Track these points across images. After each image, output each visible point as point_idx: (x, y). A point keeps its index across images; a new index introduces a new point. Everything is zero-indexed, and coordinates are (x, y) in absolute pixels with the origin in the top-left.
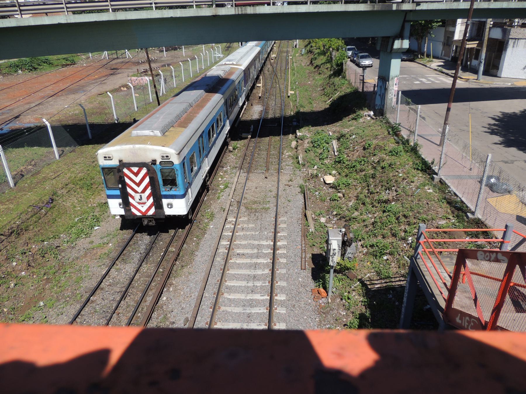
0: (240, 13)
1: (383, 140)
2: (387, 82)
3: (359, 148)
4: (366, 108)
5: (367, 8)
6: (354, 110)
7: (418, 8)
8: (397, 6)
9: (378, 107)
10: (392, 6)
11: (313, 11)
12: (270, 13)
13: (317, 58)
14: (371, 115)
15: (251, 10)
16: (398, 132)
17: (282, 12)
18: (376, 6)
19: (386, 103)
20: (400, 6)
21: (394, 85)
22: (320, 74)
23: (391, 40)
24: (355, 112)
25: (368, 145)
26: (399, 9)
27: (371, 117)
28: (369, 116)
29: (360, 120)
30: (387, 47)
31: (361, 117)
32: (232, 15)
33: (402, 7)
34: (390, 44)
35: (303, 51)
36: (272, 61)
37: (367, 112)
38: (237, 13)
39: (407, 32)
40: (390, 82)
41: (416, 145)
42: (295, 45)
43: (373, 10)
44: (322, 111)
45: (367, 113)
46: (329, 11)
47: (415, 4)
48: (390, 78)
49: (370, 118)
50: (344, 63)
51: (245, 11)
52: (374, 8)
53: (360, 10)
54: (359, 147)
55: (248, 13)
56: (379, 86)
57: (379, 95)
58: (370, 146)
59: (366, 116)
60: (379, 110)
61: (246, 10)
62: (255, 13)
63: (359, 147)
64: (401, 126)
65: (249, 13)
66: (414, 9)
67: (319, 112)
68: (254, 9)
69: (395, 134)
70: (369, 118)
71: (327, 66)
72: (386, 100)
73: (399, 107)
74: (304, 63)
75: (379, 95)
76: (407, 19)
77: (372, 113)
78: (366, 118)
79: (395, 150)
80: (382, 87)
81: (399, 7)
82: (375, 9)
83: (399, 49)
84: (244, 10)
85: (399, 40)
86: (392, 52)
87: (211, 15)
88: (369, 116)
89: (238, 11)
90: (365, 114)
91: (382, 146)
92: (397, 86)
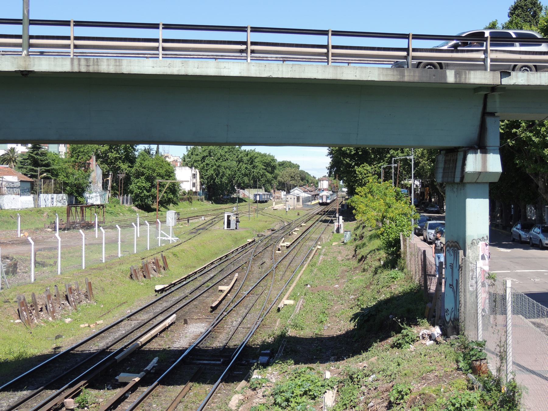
0: (83, 69)
1: (439, 382)
2: (461, 252)
3: (379, 404)
4: (425, 321)
5: (387, 75)
6: (395, 323)
7: (506, 81)
8: (457, 74)
9: (449, 316)
10: (445, 76)
11: (258, 76)
12: (161, 73)
13: (367, 244)
14: (436, 335)
15: (108, 65)
16: (478, 363)
17: (182, 72)
18: (406, 73)
19: (462, 302)
20: (463, 76)
21: (478, 259)
22: (364, 270)
23: (460, 156)
24: (399, 330)
25: (396, 395)
26: (463, 81)
27: (435, 340)
28: (431, 337)
29: (409, 348)
30: (455, 172)
31: (413, 341)
32: (65, 72)
33: (469, 79)
34: (459, 164)
35: (347, 236)
36: (277, 252)
37: (427, 329)
38: (76, 69)
39: (493, 139)
40: (468, 251)
41: (513, 389)
42: (335, 229)
43: (401, 80)
44: (338, 337)
45: (428, 332)
46: (297, 76)
47: (498, 74)
48: (468, 242)
49: (432, 342)
50: (401, 238)
51: (96, 67)
52: (404, 76)
53: (369, 79)
54: (380, 401)
55: (102, 71)
56: (448, 265)
57: (450, 285)
58: (402, 398)
59: (423, 338)
60: (452, 322)
61: (98, 65)
62: (119, 71)
63: (380, 401)
64: (487, 350)
65: (106, 71)
66: (497, 82)
67: (332, 339)
68: (118, 64)
69: (470, 368)
70: (429, 343)
71: (380, 256)
72: (462, 294)
73: (509, 322)
74: (342, 257)
75: (450, 285)
76: (489, 110)
77: (437, 331)
78: (424, 342)
79: (454, 401)
80: (455, 265)
81: (460, 77)
82: (406, 79)
83: (480, 173)
84: (94, 65)
85: (476, 153)
86: (466, 180)
87: (14, 70)
88: (431, 337)
89: (79, 65)
90: (421, 334)
91: (430, 396)
92: (487, 261)
